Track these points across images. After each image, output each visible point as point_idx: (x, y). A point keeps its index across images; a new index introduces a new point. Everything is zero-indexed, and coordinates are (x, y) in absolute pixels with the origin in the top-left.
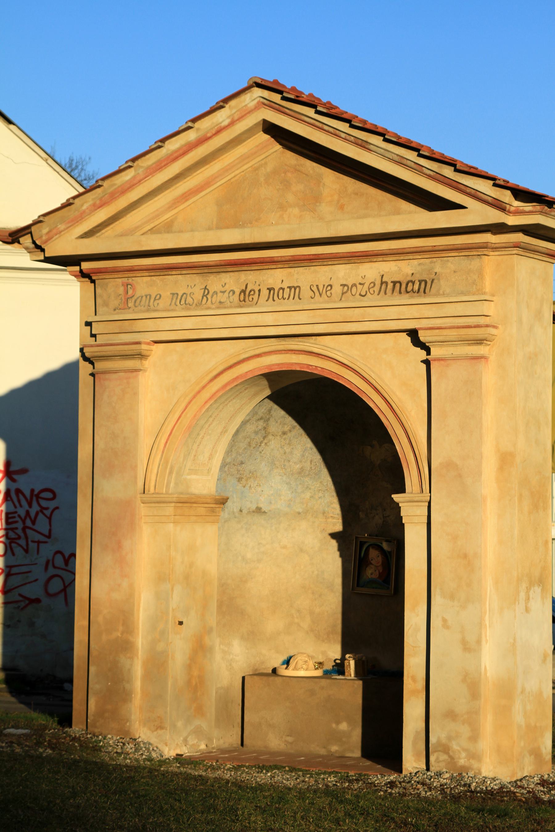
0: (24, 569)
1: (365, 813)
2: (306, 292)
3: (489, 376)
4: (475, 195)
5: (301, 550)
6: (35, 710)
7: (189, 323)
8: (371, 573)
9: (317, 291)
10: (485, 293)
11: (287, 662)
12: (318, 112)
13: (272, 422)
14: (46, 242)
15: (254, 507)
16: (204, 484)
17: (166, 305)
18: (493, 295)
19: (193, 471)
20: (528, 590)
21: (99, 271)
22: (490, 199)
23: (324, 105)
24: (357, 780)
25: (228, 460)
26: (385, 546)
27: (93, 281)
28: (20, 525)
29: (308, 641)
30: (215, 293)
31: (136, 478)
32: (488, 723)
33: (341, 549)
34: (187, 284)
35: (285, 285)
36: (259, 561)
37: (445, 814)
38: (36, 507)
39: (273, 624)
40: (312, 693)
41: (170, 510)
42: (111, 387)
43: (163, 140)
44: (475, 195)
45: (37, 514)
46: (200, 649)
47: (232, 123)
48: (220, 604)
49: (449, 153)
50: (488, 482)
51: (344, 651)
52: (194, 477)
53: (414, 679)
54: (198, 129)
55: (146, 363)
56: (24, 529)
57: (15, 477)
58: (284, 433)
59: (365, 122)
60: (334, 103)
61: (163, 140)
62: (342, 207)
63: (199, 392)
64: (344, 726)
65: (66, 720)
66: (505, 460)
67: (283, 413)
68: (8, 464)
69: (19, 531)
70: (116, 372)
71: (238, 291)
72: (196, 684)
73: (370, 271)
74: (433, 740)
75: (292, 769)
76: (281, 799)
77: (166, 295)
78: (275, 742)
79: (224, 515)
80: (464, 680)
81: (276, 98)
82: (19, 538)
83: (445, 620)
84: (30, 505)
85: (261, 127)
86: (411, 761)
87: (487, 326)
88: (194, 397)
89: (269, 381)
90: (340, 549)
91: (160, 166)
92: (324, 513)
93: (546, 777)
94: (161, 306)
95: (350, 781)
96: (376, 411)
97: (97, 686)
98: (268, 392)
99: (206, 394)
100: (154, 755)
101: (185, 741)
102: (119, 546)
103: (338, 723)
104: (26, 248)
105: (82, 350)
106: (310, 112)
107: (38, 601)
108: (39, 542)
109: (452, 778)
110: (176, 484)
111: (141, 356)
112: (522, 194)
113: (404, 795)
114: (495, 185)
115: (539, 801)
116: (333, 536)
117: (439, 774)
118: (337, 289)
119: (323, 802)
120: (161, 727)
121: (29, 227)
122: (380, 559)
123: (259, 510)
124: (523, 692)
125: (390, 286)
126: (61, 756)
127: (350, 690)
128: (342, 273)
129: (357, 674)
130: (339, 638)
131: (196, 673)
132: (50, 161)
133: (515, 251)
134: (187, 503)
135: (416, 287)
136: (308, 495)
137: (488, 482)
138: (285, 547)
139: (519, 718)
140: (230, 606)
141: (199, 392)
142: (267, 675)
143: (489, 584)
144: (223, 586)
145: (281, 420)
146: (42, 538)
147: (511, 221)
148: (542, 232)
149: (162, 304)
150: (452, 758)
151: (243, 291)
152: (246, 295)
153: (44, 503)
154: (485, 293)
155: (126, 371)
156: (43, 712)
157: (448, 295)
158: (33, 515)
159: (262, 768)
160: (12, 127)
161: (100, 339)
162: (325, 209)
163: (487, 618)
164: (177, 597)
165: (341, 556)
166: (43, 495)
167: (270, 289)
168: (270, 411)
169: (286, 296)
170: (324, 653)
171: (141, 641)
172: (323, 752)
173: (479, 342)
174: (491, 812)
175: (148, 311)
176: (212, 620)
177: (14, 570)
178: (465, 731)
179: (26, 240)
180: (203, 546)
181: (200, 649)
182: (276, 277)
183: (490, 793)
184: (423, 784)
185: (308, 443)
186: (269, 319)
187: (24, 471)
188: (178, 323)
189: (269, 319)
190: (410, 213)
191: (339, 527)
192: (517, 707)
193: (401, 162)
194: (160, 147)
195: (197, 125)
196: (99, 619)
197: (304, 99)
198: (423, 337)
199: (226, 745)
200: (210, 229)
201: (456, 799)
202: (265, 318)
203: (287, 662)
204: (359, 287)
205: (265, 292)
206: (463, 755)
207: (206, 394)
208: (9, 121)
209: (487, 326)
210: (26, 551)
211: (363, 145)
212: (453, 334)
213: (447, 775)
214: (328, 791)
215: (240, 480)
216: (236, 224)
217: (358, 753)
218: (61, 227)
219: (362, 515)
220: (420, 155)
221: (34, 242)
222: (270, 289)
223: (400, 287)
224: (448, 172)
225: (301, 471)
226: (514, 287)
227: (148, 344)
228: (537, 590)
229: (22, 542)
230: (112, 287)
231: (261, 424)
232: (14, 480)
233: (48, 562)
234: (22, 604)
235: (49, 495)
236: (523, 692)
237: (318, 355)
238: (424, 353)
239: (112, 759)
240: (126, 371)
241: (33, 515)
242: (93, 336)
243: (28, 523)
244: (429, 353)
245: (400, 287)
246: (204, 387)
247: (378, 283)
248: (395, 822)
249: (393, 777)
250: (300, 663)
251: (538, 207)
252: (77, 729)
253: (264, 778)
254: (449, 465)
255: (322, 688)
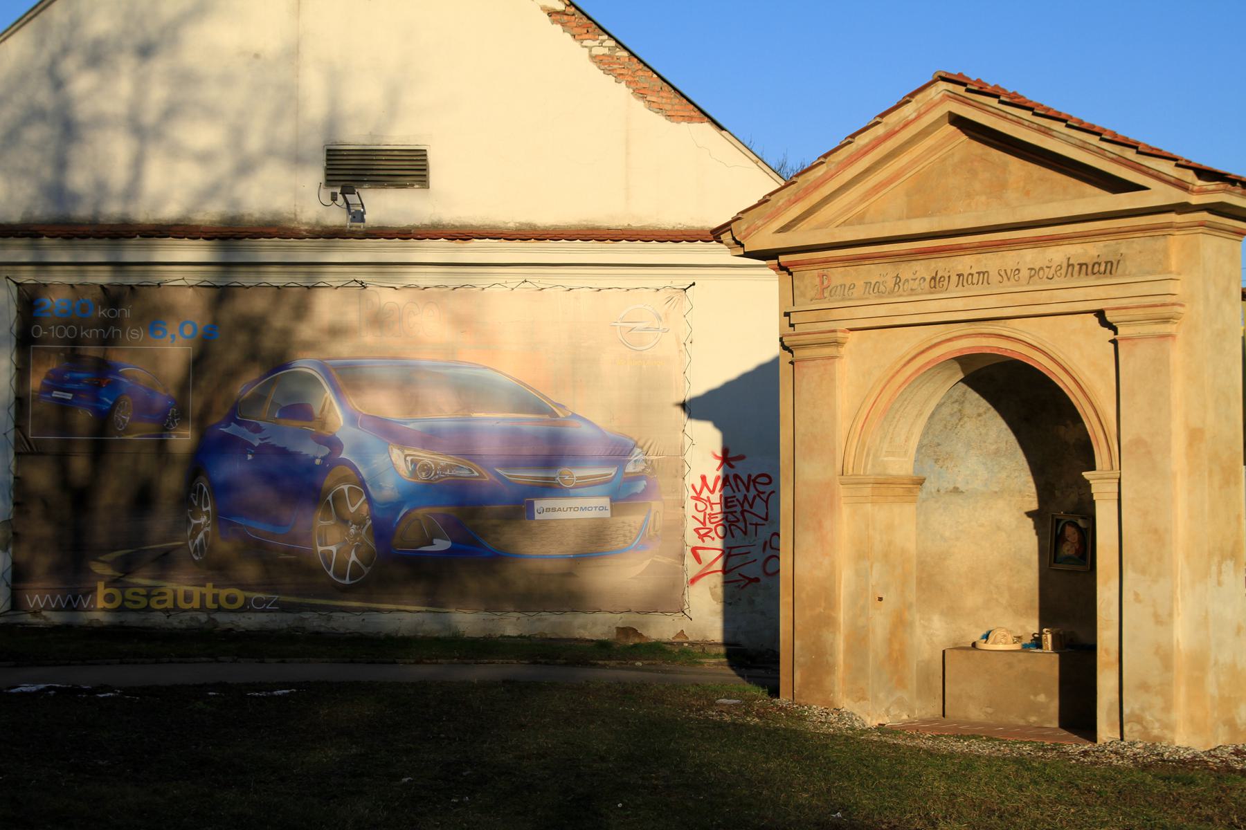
0: (743, 550)
1: (1050, 780)
2: (994, 277)
3: (1176, 354)
4: (1158, 176)
5: (999, 528)
6: (749, 682)
7: (882, 310)
8: (1068, 549)
9: (1005, 275)
10: (1171, 272)
11: (987, 637)
12: (1001, 102)
13: (967, 405)
14: (745, 238)
15: (951, 487)
16: (901, 465)
17: (859, 292)
18: (1179, 274)
19: (890, 453)
20: (1220, 563)
21: (796, 264)
22: (1172, 180)
23: (1008, 95)
24: (1052, 749)
25: (925, 442)
26: (1081, 523)
27: (790, 274)
28: (739, 509)
29: (1009, 619)
30: (907, 280)
31: (834, 459)
32: (1181, 695)
33: (1037, 527)
34: (879, 273)
35: (974, 271)
36: (957, 539)
37: (1130, 782)
38: (753, 492)
39: (972, 600)
40: (1010, 666)
41: (867, 490)
42: (809, 376)
43: (853, 136)
44: (1158, 176)
45: (754, 498)
46: (900, 624)
47: (918, 117)
48: (920, 581)
49: (1133, 136)
50: (1178, 458)
51: (1042, 626)
52: (891, 458)
53: (1107, 651)
54: (886, 124)
55: (843, 350)
56: (742, 513)
57: (733, 463)
58: (979, 415)
59: (1081, 122)
60: (1020, 93)
61: (853, 136)
62: (1027, 193)
63: (893, 377)
64: (1042, 698)
65: (775, 692)
66: (1195, 436)
67: (977, 395)
68: (725, 451)
69: (738, 515)
70: (814, 359)
71: (928, 278)
72: (896, 658)
73: (1057, 255)
74: (1126, 710)
75: (989, 739)
76: (969, 766)
77: (860, 284)
78: (976, 713)
79: (921, 495)
80: (1157, 653)
81: (961, 90)
82: (738, 520)
83: (1136, 594)
84: (748, 490)
85: (947, 119)
86: (1106, 731)
87: (1173, 304)
88: (889, 381)
89: (961, 364)
90: (1035, 527)
91: (851, 161)
92: (1020, 492)
93: (1240, 747)
94: (855, 295)
95: (1045, 751)
96: (1066, 390)
97: (802, 659)
98: (961, 376)
99: (900, 378)
100: (857, 724)
101: (887, 711)
102: (820, 523)
103: (1036, 695)
104: (727, 245)
105: (781, 340)
106: (993, 102)
107: (757, 580)
108: (756, 525)
109: (1145, 748)
110: (873, 466)
111: (837, 344)
112: (1205, 174)
113: (1096, 763)
114: (1177, 165)
115: (1230, 769)
116: (1029, 514)
117: (1133, 744)
118: (1025, 273)
119: (1010, 769)
120: (863, 698)
121: (728, 224)
122: (1076, 536)
123: (956, 490)
124: (1216, 663)
125: (1077, 268)
126: (768, 725)
127: (1048, 663)
128: (1029, 257)
129: (1054, 647)
130: (1036, 613)
131: (896, 646)
132: (760, 163)
133: (1200, 229)
134: (884, 485)
135: (1102, 269)
136: (1004, 474)
137: (1178, 458)
138: (982, 525)
139: (1212, 689)
140: (929, 581)
141: (893, 377)
142: (967, 649)
143: (1180, 560)
144: (237, 402)
145: (976, 402)
146: (760, 521)
147: (1195, 200)
148: (1226, 210)
149: (856, 293)
150: (1145, 728)
151: (934, 278)
152: (936, 282)
153: (761, 488)
154: (1171, 272)
155: (823, 358)
156: (757, 684)
157: (1135, 275)
158: (750, 499)
159: (960, 737)
160: (724, 132)
161: (798, 329)
162: (1011, 195)
163: (1179, 591)
164: (876, 575)
165: (1037, 534)
166: (759, 480)
167: (959, 275)
168: (964, 394)
169: (975, 281)
170: (1022, 628)
171: (842, 616)
172: (1022, 722)
173: (1166, 320)
174: (1177, 780)
175: (843, 300)
176: (912, 596)
177: (734, 551)
178: (1158, 701)
179: (727, 237)
180: (902, 525)
181: (900, 624)
182: (965, 263)
183: (1183, 762)
184: (1116, 753)
185: (1004, 425)
186: (959, 304)
187: (741, 458)
188: (871, 311)
189: (959, 304)
190: (1095, 195)
191: (1034, 506)
192: (1210, 678)
193: (1083, 147)
194: (850, 143)
195: (885, 120)
196: (801, 595)
197: (989, 89)
198: (1110, 317)
199: (928, 716)
200: (900, 219)
201: (1146, 767)
202: (955, 303)
203: (987, 637)
204: (1047, 270)
205: (954, 279)
206: (1157, 725)
207: (900, 378)
208: (722, 128)
209: (1173, 304)
210: (745, 533)
211: (1046, 132)
212: (1140, 313)
213: (1140, 745)
214: (1020, 761)
215: (937, 461)
216: (925, 213)
217: (1056, 724)
218: (759, 223)
219: (1057, 493)
220: (1102, 139)
221: (734, 238)
222: (959, 275)
223: (1087, 269)
224: (1130, 154)
225: (997, 452)
226: (1200, 265)
227: (843, 331)
228: (1229, 565)
229: (741, 525)
230: (809, 279)
231: (956, 406)
232: (731, 466)
233: (765, 543)
234: (743, 583)
235: (765, 480)
236: (1216, 663)
237: (1008, 338)
238: (1112, 332)
239: (816, 728)
240: (823, 358)
241: (750, 499)
242: (792, 325)
243: (747, 507)
244: (1116, 333)
245: (1087, 269)
246: (898, 372)
247: (1064, 265)
248: (1078, 789)
249: (1087, 746)
250: (999, 637)
251: (1221, 185)
252: (784, 699)
253: (961, 746)
254: (1139, 442)
255: (1020, 661)
